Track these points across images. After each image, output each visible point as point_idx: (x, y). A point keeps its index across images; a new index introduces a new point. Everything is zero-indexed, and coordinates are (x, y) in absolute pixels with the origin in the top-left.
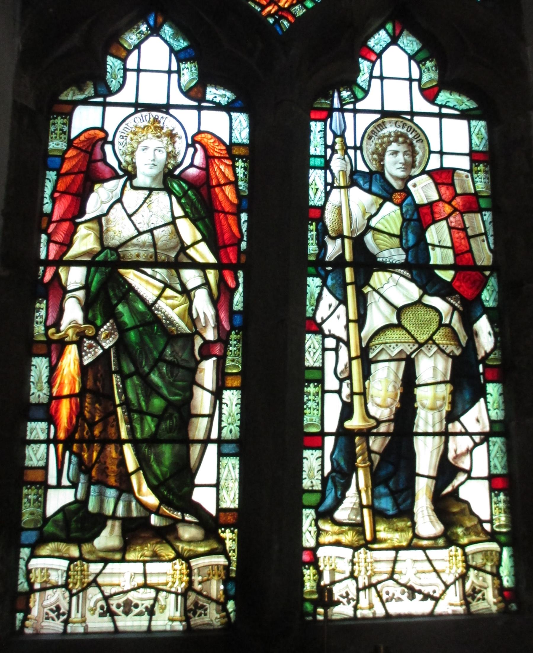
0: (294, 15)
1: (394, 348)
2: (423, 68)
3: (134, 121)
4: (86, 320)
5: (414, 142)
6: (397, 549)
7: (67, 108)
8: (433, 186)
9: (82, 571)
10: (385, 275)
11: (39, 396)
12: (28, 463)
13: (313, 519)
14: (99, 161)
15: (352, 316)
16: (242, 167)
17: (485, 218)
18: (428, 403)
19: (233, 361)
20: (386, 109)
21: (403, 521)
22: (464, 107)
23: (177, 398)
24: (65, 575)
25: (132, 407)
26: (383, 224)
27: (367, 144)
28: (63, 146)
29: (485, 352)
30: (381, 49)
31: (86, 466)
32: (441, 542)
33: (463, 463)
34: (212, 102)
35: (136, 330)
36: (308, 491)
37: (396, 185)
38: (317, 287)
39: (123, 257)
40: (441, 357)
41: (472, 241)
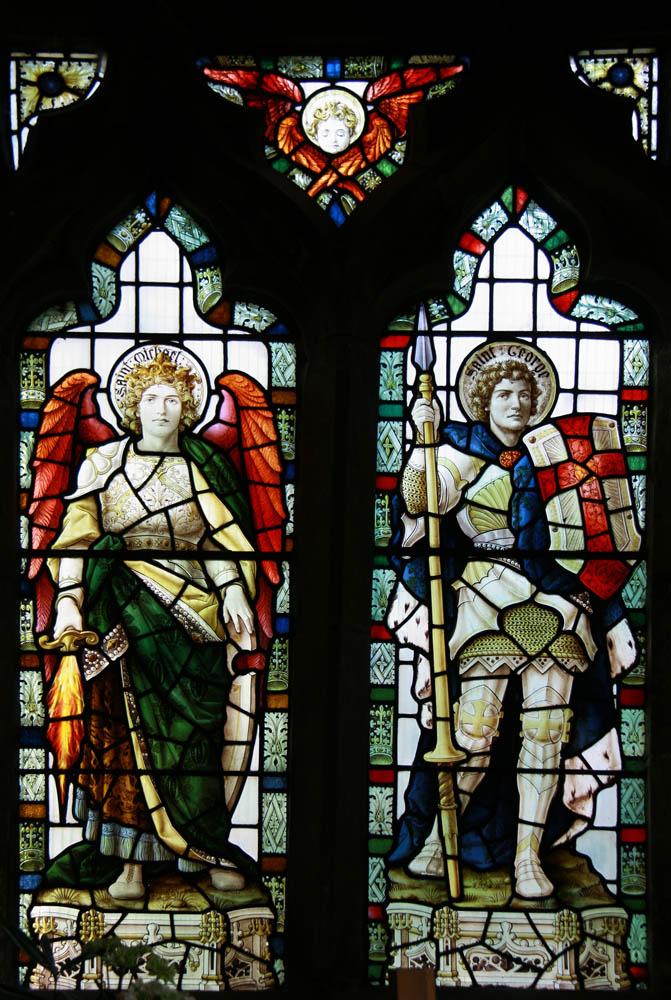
0: (361, 188)
1: (493, 661)
2: (556, 261)
3: (135, 359)
4: (86, 625)
5: (536, 376)
6: (490, 910)
7: (41, 343)
8: (560, 440)
9: (96, 921)
10: (484, 567)
11: (32, 718)
12: (23, 797)
13: (382, 869)
14: (90, 416)
15: (437, 619)
16: (286, 421)
17: (635, 484)
18: (539, 734)
19: (278, 676)
20: (496, 328)
21: (502, 876)
22: (616, 320)
23: (207, 721)
24: (75, 925)
25: (149, 731)
26: (484, 497)
27: (465, 383)
28: (40, 396)
29: (623, 668)
30: (493, 234)
31: (95, 802)
32: (549, 904)
33: (583, 808)
34: (242, 328)
35: (151, 638)
36: (375, 836)
37: (505, 439)
38: (389, 582)
39: (130, 545)
40: (559, 674)
41: (613, 518)
